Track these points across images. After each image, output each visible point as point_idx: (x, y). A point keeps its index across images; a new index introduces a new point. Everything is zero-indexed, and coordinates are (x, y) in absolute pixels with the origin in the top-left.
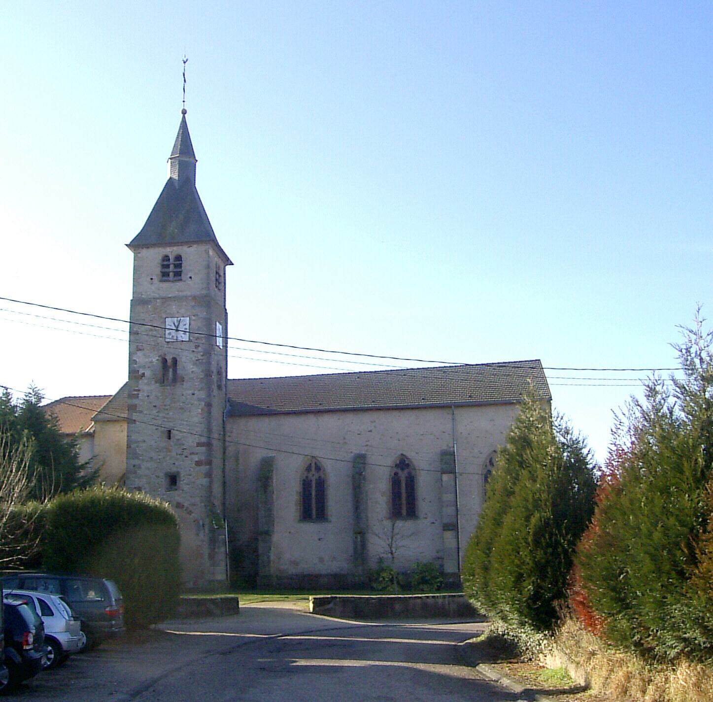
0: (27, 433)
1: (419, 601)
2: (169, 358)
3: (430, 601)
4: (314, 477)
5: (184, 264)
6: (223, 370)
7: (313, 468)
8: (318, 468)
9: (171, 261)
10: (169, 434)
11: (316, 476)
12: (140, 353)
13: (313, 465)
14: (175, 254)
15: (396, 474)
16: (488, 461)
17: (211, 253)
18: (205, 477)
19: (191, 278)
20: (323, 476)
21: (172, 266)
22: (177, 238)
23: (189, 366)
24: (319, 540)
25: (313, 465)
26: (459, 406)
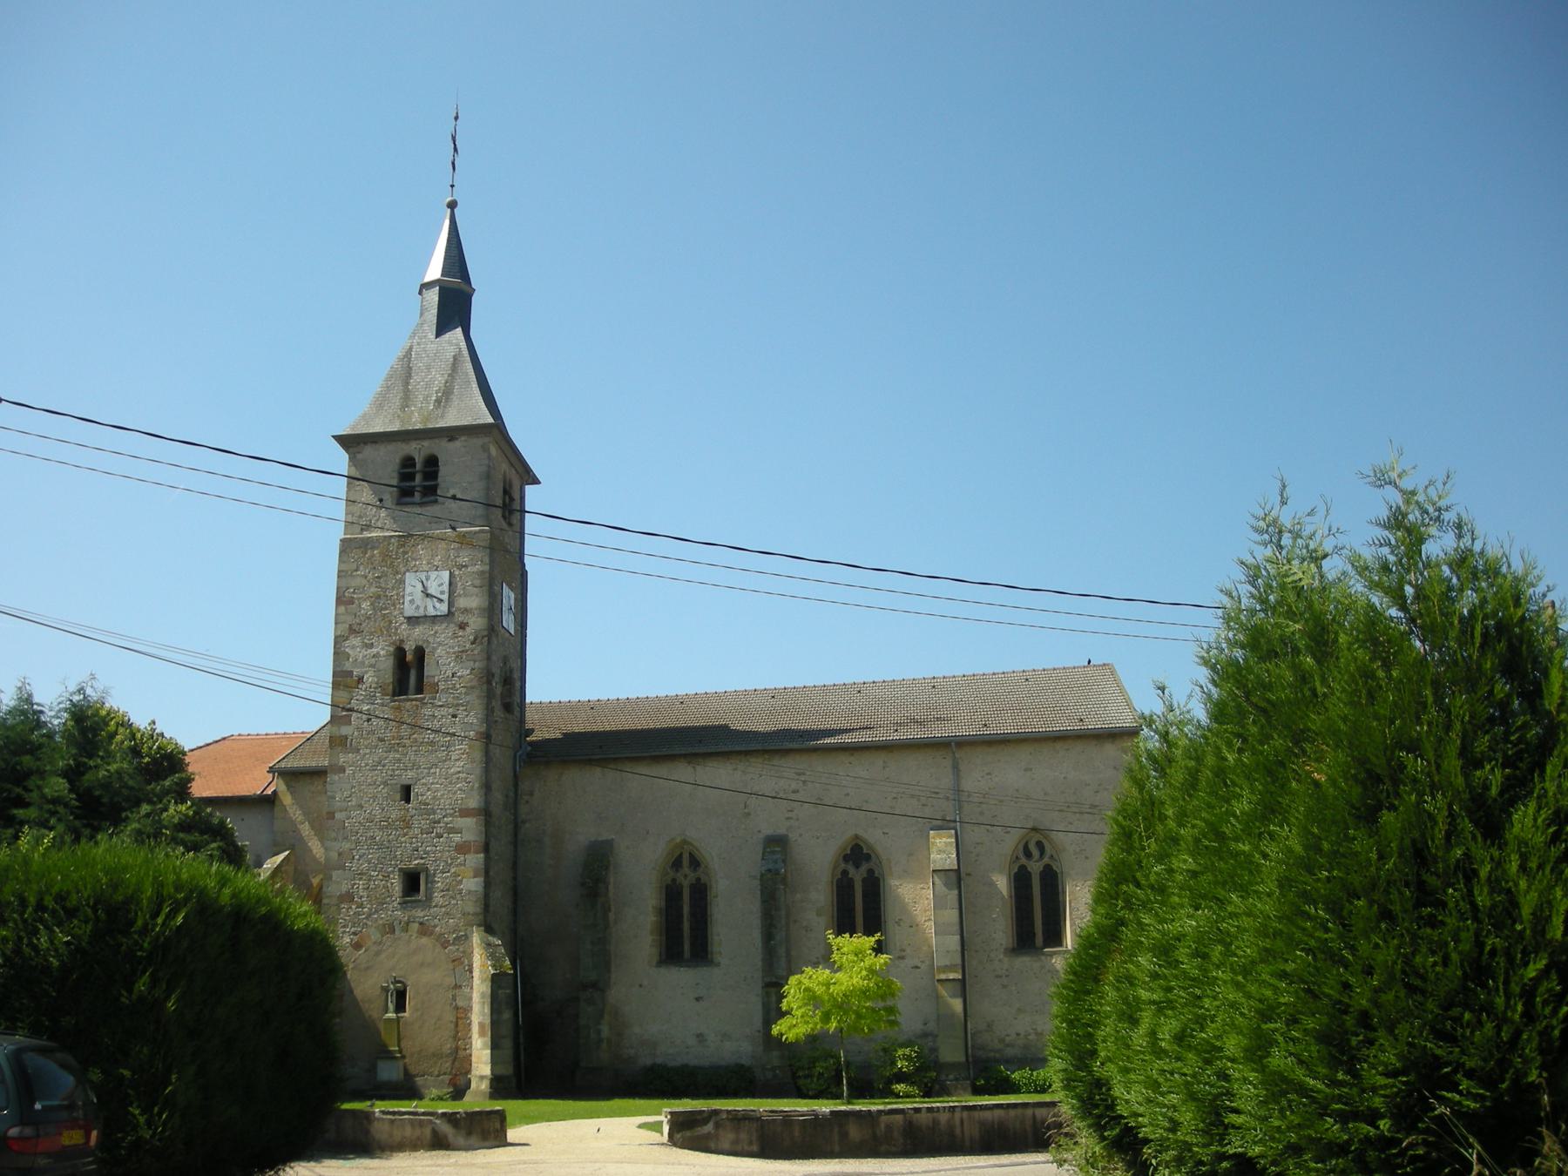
0: (93, 770)
1: (899, 1117)
2: (409, 647)
3: (924, 1118)
4: (686, 878)
5: (443, 471)
6: (516, 675)
7: (686, 862)
8: (695, 863)
9: (418, 466)
11: (692, 876)
12: (355, 641)
13: (686, 857)
14: (425, 453)
15: (845, 873)
16: (1021, 847)
17: (493, 451)
20: (704, 879)
21: (418, 478)
22: (441, 481)
23: (450, 663)
24: (697, 999)
25: (686, 857)
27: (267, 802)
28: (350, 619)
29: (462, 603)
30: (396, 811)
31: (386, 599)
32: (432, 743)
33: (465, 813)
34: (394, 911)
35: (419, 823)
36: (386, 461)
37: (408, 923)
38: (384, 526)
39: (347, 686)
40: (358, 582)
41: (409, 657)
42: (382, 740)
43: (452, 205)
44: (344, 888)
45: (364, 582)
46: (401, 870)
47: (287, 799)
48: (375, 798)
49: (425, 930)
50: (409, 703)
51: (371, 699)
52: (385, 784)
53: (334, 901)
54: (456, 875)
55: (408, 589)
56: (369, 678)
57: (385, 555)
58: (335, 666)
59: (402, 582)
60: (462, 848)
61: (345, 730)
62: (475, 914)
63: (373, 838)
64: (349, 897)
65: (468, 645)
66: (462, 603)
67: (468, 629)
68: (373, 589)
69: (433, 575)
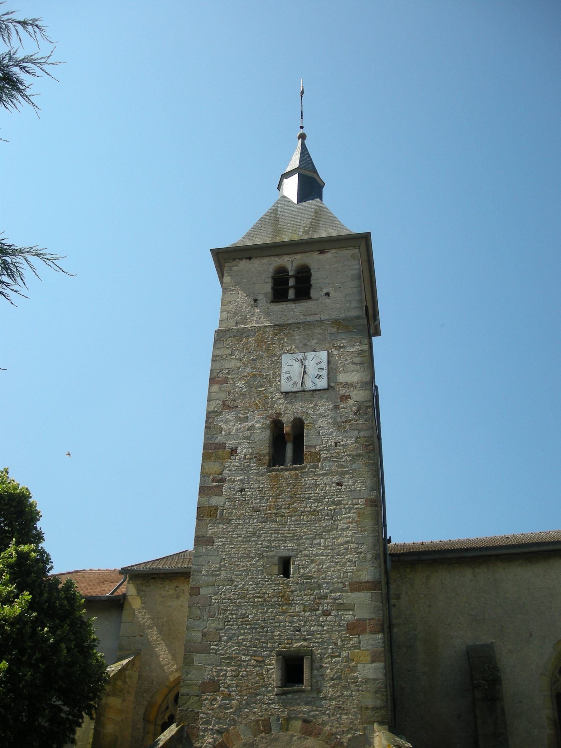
10: (285, 566)
12: (228, 416)
18: (373, 662)
19: (328, 294)
26: (170, 691)
27: (116, 604)
28: (223, 396)
29: (342, 378)
30: (272, 586)
31: (262, 380)
32: (315, 512)
33: (356, 587)
34: (270, 705)
35: (302, 599)
36: (263, 270)
37: (288, 720)
38: (259, 318)
39: (218, 458)
40: (233, 364)
41: (287, 429)
42: (257, 510)
43: (302, 137)
44: (207, 676)
45: (239, 364)
46: (279, 654)
47: (136, 603)
48: (247, 571)
49: (310, 728)
50: (287, 474)
51: (245, 469)
52: (260, 556)
53: (195, 690)
54: (349, 659)
55: (285, 368)
56: (243, 450)
57: (260, 342)
58: (206, 439)
59: (279, 362)
60: (355, 628)
61: (215, 501)
62: (375, 709)
63: (245, 616)
64: (213, 686)
65: (351, 416)
66: (342, 378)
67: (350, 402)
68: (248, 370)
69: (310, 355)
